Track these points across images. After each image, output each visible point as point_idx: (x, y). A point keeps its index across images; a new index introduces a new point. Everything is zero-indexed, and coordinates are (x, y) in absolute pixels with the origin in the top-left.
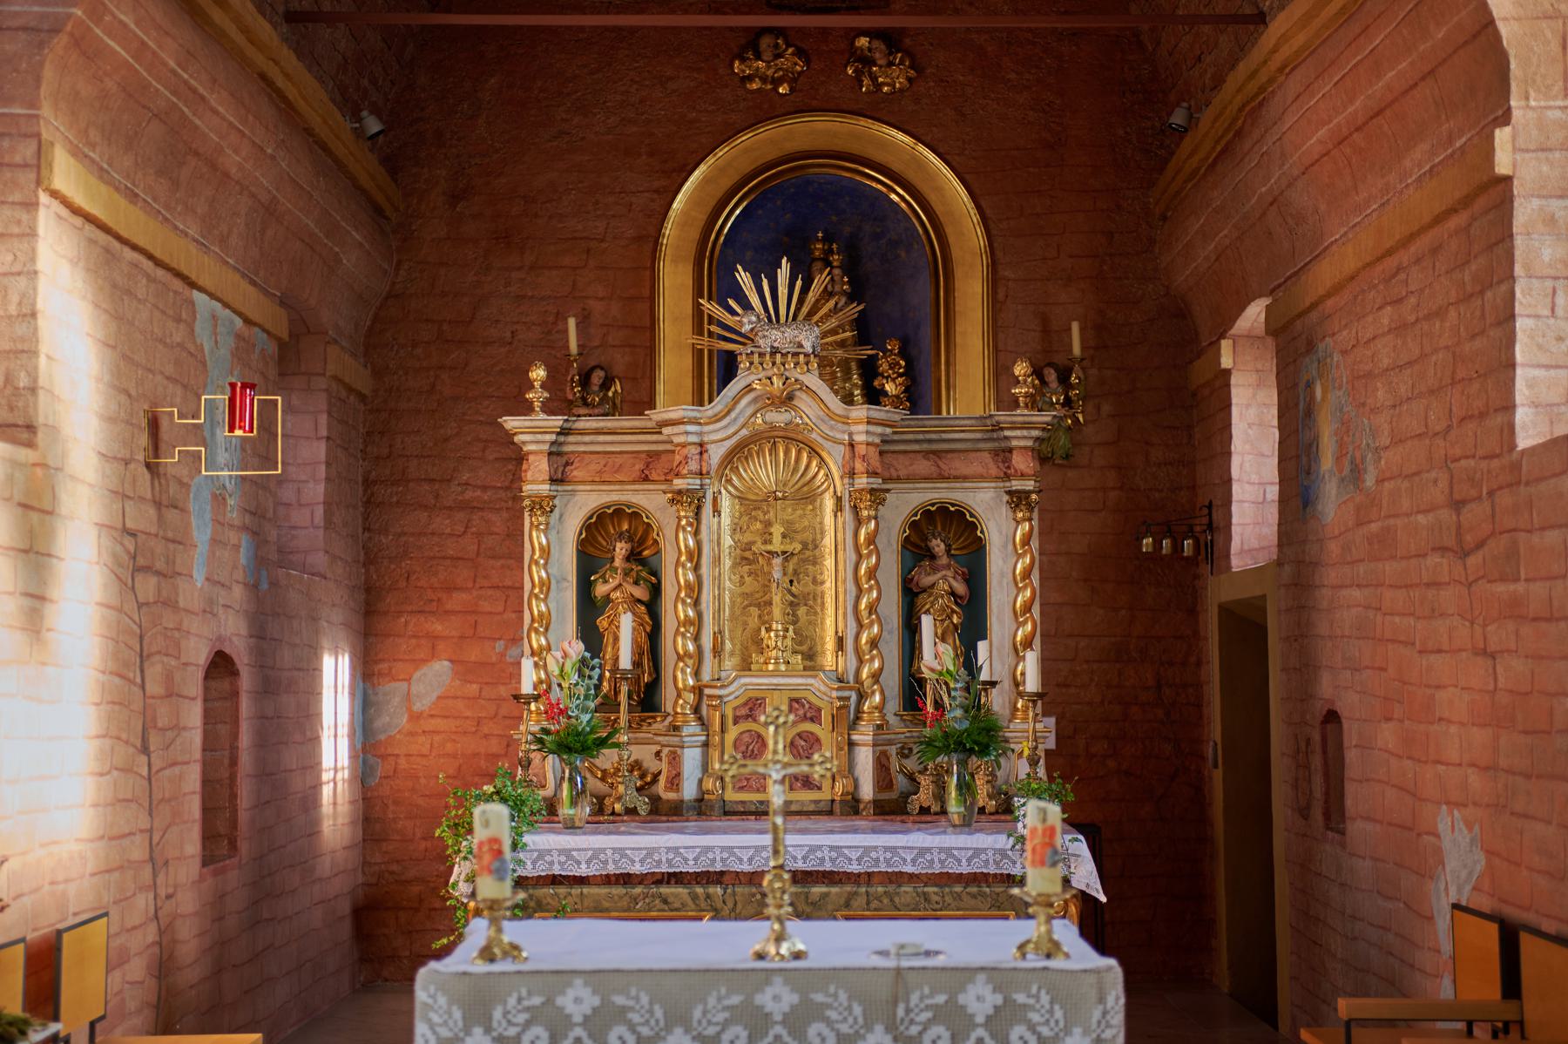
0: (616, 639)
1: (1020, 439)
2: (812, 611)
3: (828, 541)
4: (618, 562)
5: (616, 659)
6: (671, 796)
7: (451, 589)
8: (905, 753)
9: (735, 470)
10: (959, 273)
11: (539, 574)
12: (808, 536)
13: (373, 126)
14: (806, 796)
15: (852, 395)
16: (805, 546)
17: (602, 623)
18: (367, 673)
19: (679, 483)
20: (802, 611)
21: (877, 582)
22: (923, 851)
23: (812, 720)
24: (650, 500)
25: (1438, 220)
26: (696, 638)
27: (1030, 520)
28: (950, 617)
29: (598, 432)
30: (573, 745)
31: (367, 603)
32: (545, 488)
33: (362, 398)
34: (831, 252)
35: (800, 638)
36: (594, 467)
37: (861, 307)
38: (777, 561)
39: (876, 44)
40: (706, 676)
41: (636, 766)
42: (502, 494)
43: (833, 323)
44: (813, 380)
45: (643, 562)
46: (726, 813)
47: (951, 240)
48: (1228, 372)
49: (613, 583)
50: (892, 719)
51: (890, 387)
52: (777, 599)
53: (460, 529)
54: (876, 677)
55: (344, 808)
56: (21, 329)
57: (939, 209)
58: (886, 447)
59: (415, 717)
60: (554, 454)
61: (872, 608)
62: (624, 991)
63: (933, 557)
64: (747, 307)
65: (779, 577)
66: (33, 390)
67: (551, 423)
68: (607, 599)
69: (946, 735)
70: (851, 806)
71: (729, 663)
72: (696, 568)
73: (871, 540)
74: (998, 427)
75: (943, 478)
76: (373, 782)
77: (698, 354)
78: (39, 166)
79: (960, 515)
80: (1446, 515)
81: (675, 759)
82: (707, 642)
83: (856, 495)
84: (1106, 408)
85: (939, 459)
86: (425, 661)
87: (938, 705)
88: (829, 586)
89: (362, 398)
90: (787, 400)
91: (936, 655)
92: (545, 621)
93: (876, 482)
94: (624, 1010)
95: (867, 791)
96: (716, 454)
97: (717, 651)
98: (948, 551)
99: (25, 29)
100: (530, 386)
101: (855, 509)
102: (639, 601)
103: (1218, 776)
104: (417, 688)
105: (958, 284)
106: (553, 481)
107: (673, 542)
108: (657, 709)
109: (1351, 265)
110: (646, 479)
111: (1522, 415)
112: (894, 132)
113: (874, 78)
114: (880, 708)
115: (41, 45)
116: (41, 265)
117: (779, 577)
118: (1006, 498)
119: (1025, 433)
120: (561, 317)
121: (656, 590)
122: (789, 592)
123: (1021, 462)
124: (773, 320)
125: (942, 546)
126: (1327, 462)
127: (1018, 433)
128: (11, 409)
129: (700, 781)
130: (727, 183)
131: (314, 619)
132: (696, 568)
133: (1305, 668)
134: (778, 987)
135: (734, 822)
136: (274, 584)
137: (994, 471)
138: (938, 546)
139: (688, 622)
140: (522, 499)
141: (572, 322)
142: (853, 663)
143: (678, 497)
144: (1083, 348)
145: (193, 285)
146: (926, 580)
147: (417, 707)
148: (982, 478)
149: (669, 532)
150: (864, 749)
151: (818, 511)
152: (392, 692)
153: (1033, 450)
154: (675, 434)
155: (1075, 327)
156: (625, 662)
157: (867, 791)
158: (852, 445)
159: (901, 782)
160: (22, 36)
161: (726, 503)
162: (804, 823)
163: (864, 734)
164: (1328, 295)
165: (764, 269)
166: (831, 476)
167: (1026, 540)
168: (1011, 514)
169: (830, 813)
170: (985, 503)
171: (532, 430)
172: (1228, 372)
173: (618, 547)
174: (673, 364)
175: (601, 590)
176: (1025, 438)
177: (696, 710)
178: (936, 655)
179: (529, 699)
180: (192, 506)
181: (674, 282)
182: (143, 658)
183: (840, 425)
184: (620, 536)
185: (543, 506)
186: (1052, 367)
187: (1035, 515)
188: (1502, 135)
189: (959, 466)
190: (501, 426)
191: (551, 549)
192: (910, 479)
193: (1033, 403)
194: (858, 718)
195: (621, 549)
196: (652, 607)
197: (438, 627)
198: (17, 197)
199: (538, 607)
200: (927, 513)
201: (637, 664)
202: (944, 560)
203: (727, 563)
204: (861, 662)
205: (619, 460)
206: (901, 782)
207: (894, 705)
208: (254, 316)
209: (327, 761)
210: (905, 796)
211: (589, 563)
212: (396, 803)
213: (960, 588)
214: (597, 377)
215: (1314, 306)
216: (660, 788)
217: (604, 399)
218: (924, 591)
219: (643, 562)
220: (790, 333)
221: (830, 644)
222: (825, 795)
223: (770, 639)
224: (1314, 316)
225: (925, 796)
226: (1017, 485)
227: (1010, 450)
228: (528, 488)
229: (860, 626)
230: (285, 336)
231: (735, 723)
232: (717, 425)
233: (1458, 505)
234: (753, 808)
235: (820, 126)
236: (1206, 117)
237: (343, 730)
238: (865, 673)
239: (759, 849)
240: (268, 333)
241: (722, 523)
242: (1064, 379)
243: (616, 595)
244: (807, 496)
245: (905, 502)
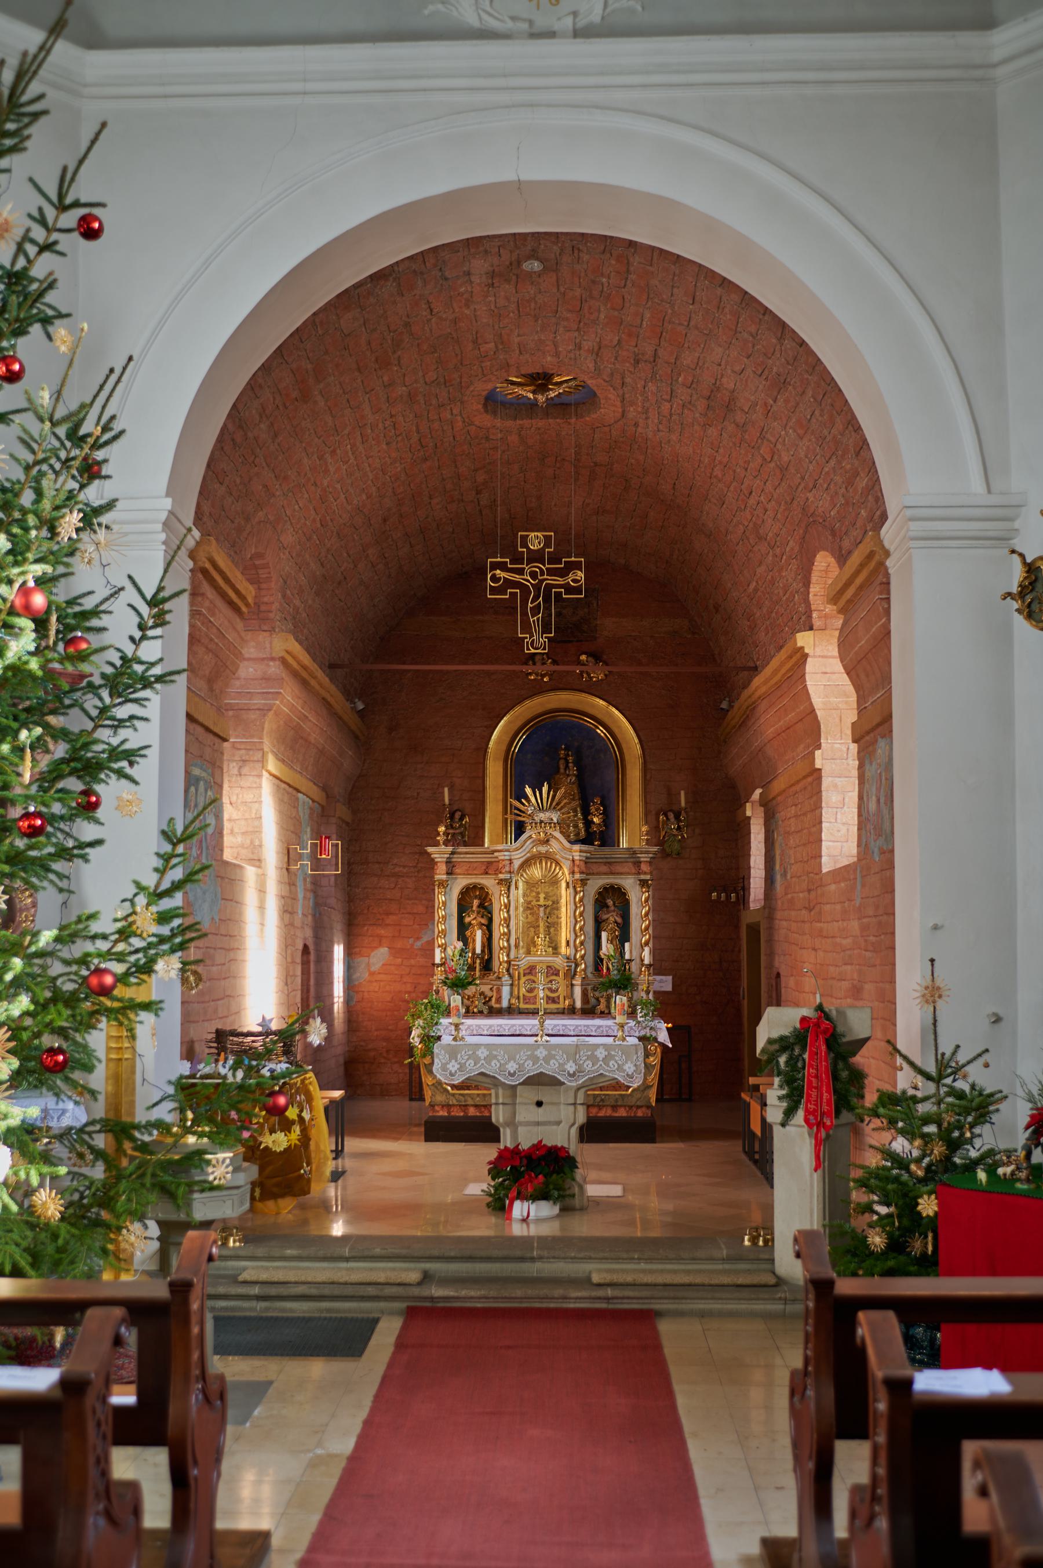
0: (474, 941)
2: (556, 930)
3: (563, 901)
4: (474, 908)
5: (474, 949)
6: (497, 1006)
7: (388, 914)
8: (594, 989)
9: (524, 871)
10: (628, 767)
11: (442, 913)
12: (554, 898)
13: (360, 706)
14: (553, 1006)
16: (554, 902)
17: (468, 933)
18: (350, 954)
19: (501, 876)
20: (552, 930)
22: (599, 1027)
24: (489, 882)
25: (805, 777)
26: (508, 941)
29: (467, 853)
30: (458, 985)
31: (349, 920)
32: (444, 877)
33: (347, 824)
34: (568, 755)
35: (551, 941)
36: (465, 868)
38: (542, 909)
39: (590, 659)
40: (512, 956)
41: (482, 994)
42: (412, 869)
44: (557, 834)
45: (485, 908)
47: (625, 751)
48: (749, 818)
49: (472, 917)
50: (590, 975)
51: (596, 820)
52: (541, 924)
53: (393, 886)
54: (583, 957)
55: (341, 1015)
56: (256, 823)
57: (619, 736)
59: (372, 974)
60: (448, 862)
61: (581, 929)
62: (496, 1050)
63: (608, 907)
65: (543, 915)
66: (261, 846)
68: (470, 924)
69: (610, 981)
70: (571, 1011)
71: (521, 951)
72: (508, 912)
73: (581, 900)
75: (612, 873)
76: (352, 1003)
78: (263, 761)
79: (619, 889)
80: (806, 894)
81: (499, 991)
82: (512, 942)
83: (575, 882)
84: (697, 831)
85: (611, 866)
86: (376, 948)
87: (608, 969)
88: (563, 920)
89: (347, 824)
90: (547, 842)
91: (607, 948)
92: (444, 933)
93: (584, 876)
94: (496, 1056)
95: (578, 1004)
96: (517, 864)
97: (517, 946)
99: (259, 709)
100: (439, 834)
101: (575, 888)
103: (745, 1002)
104: (373, 960)
105: (628, 793)
106: (448, 874)
107: (498, 900)
108: (491, 970)
109: (783, 786)
110: (487, 873)
111: (824, 860)
112: (598, 700)
113: (588, 674)
114: (585, 970)
115: (264, 715)
116: (263, 799)
117: (543, 915)
120: (441, 786)
121: (490, 920)
123: (644, 867)
124: (541, 809)
126: (777, 867)
128: (253, 853)
130: (519, 723)
131: (332, 928)
132: (508, 912)
133: (771, 955)
134: (541, 1049)
135: (524, 1016)
136: (320, 914)
137: (634, 871)
138: (610, 902)
139: (504, 934)
140: (850, 1203)
142: (573, 951)
143: (501, 882)
145: (298, 791)
146: (605, 917)
147: (373, 969)
148: (629, 874)
149: (497, 895)
151: (558, 888)
152: (361, 962)
154: (501, 856)
155: (682, 793)
156: (478, 950)
157: (578, 1004)
158: (573, 861)
159: (593, 1001)
160: (258, 712)
161: (521, 885)
162: (552, 1016)
163: (577, 981)
164: (778, 795)
165: (537, 787)
166: (565, 874)
167: (647, 900)
169: (563, 1013)
171: (439, 853)
172: (749, 818)
173: (475, 902)
175: (467, 920)
177: (508, 970)
178: (607, 948)
179: (438, 965)
180: (298, 884)
182: (286, 947)
183: (568, 854)
184: (476, 897)
185: (442, 884)
188: (818, 753)
189: (618, 868)
191: (446, 902)
192: (598, 874)
194: (575, 974)
195: (476, 902)
196: (489, 928)
197: (382, 932)
198: (255, 773)
199: (441, 927)
200: (605, 888)
201: (483, 951)
202: (613, 908)
203: (521, 909)
204: (576, 951)
205: (475, 865)
206: (593, 1001)
207: (590, 969)
208: (316, 798)
209: (336, 994)
210: (594, 1007)
211: (463, 907)
212: (363, 1014)
213: (619, 920)
214: (458, 815)
215: (774, 798)
216: (493, 1002)
217: (461, 825)
219: (485, 908)
220: (548, 814)
221: (564, 943)
222: (561, 1006)
223: (539, 941)
224: (774, 802)
225: (602, 1006)
226: (643, 877)
228: (437, 877)
229: (576, 936)
230: (324, 803)
232: (516, 852)
233: (809, 891)
235: (563, 696)
236: (736, 705)
237: (341, 980)
238: (578, 956)
239: (534, 1026)
240: (289, 785)
241: (518, 893)
242: (677, 817)
243: (474, 922)
244: (555, 882)
245: (596, 884)
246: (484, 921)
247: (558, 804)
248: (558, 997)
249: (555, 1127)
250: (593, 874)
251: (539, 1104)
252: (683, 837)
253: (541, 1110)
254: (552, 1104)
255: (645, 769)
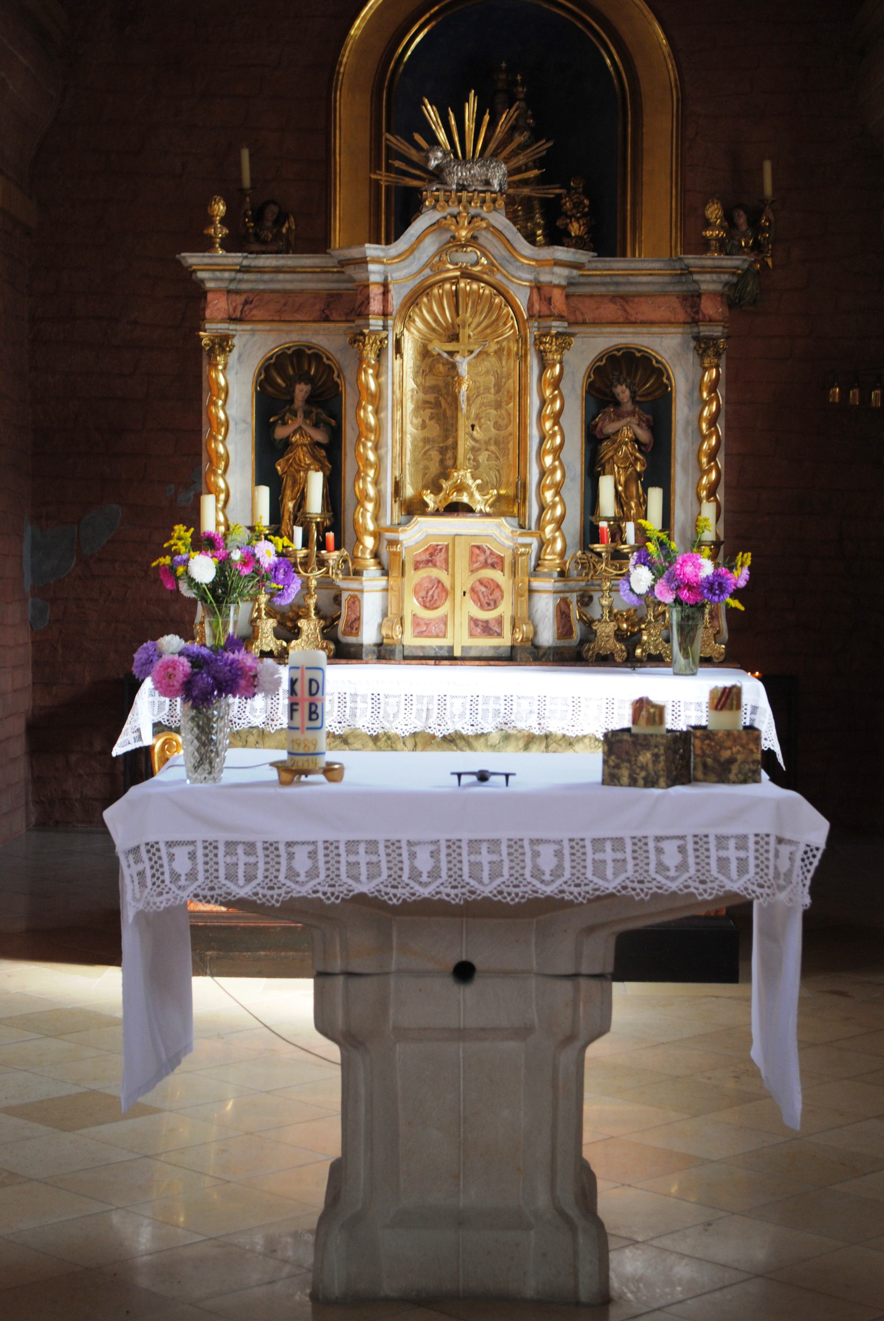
1: (709, 283)
15: (534, 235)
21: (561, 429)
23: (493, 566)
27: (717, 367)
28: (633, 465)
29: (278, 270)
37: (550, 144)
43: (521, 160)
44: (500, 220)
46: (405, 658)
58: (572, 290)
63: (617, 404)
64: (434, 141)
67: (230, 261)
70: (526, 654)
74: (687, 271)
77: (375, 185)
85: (625, 305)
95: (547, 637)
98: (633, 398)
100: (210, 221)
102: (318, 444)
105: (647, 166)
110: (327, 319)
118: (693, 344)
119: (715, 277)
122: (472, 437)
123: (709, 308)
125: (627, 392)
127: (708, 277)
129: (380, 626)
137: (682, 317)
138: (623, 392)
141: (245, 154)
144: (775, 189)
146: (610, 428)
148: (670, 323)
150: (544, 596)
153: (722, 295)
155: (767, 166)
165: (449, 103)
168: (697, 360)
170: (667, 346)
171: (214, 267)
174: (346, 202)
176: (714, 282)
181: (350, 113)
186: (742, 205)
187: (723, 361)
189: (646, 310)
190: (179, 263)
193: (724, 247)
211: (270, 405)
213: (644, 435)
214: (271, 212)
218: (608, 437)
226: (705, 330)
227: (699, 296)
231: (416, 568)
234: (432, 654)
243: (296, 438)
245: (589, 347)
246: (320, 436)
247: (503, 144)
248: (500, 621)
249: (512, 1045)
250: (584, 323)
251: (464, 972)
252: (765, 266)
253: (468, 993)
254: (505, 974)
255: (684, 118)
